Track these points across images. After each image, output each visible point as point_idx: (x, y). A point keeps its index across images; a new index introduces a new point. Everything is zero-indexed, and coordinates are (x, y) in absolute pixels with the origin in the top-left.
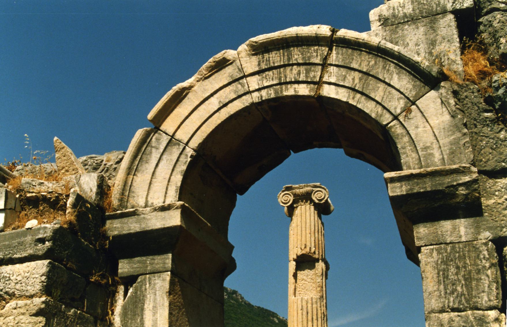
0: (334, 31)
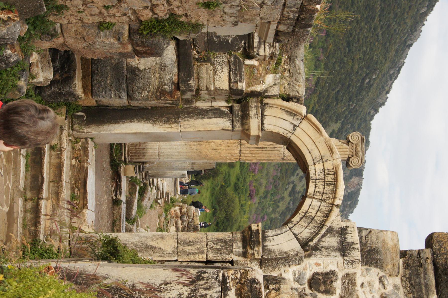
0: (337, 206)
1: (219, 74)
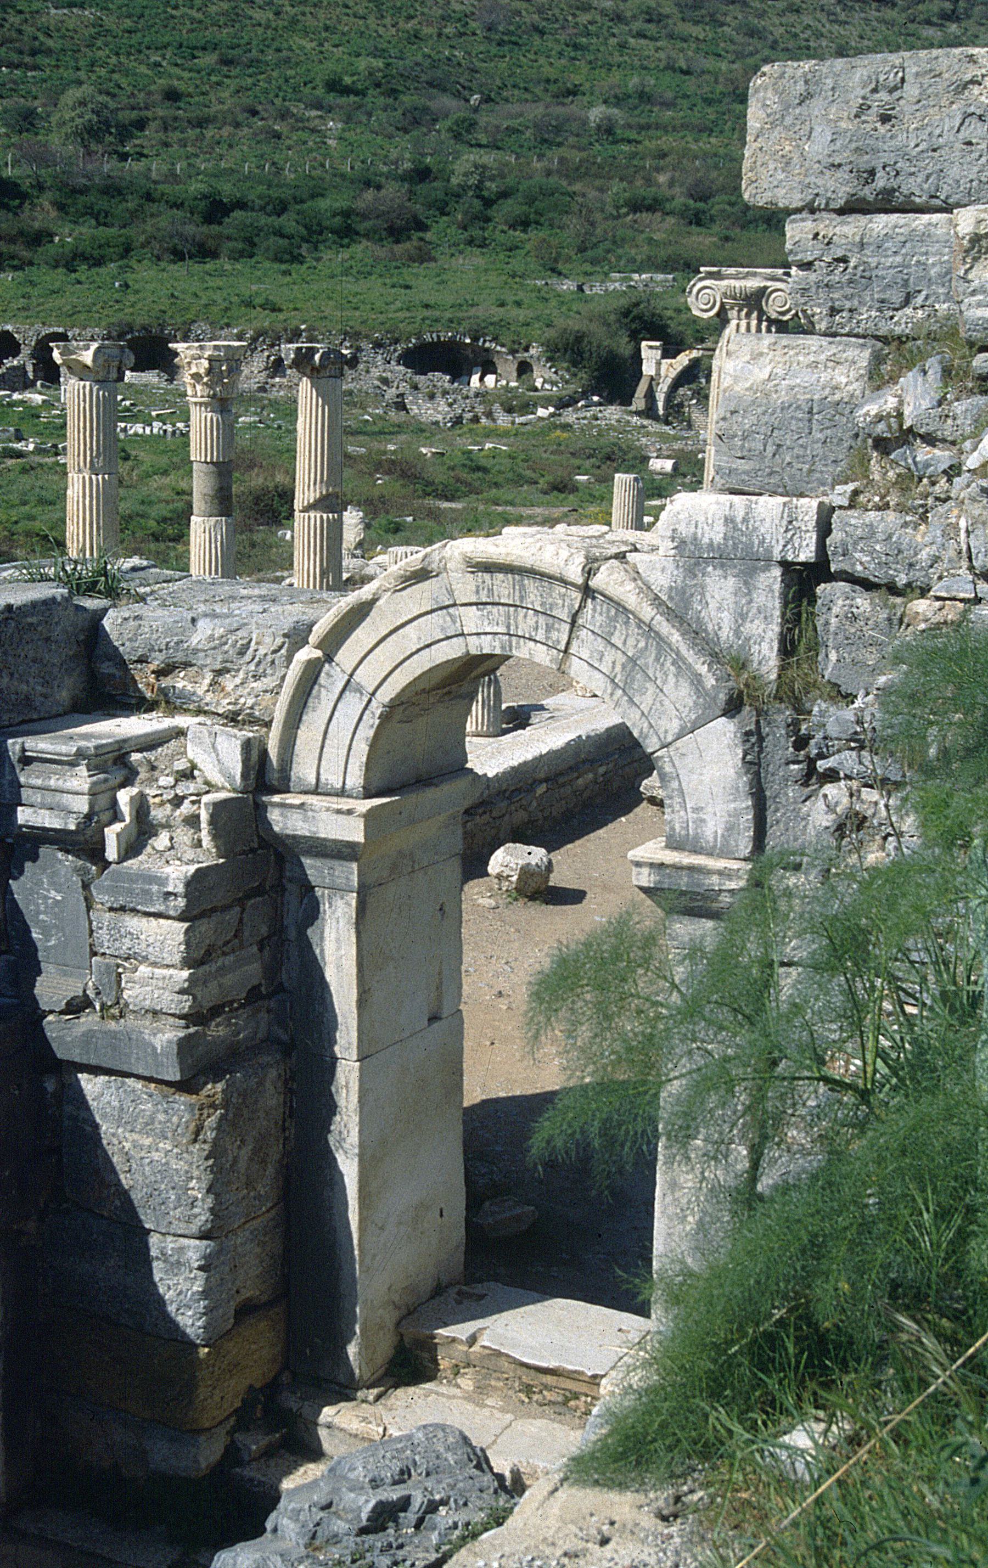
1: (143, 946)
